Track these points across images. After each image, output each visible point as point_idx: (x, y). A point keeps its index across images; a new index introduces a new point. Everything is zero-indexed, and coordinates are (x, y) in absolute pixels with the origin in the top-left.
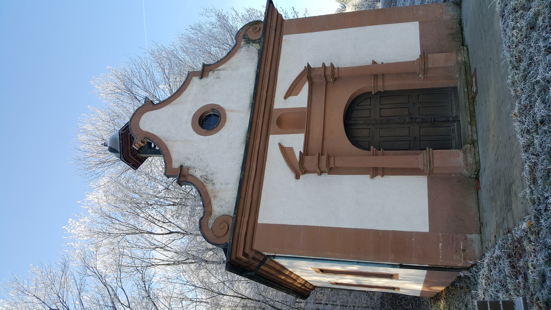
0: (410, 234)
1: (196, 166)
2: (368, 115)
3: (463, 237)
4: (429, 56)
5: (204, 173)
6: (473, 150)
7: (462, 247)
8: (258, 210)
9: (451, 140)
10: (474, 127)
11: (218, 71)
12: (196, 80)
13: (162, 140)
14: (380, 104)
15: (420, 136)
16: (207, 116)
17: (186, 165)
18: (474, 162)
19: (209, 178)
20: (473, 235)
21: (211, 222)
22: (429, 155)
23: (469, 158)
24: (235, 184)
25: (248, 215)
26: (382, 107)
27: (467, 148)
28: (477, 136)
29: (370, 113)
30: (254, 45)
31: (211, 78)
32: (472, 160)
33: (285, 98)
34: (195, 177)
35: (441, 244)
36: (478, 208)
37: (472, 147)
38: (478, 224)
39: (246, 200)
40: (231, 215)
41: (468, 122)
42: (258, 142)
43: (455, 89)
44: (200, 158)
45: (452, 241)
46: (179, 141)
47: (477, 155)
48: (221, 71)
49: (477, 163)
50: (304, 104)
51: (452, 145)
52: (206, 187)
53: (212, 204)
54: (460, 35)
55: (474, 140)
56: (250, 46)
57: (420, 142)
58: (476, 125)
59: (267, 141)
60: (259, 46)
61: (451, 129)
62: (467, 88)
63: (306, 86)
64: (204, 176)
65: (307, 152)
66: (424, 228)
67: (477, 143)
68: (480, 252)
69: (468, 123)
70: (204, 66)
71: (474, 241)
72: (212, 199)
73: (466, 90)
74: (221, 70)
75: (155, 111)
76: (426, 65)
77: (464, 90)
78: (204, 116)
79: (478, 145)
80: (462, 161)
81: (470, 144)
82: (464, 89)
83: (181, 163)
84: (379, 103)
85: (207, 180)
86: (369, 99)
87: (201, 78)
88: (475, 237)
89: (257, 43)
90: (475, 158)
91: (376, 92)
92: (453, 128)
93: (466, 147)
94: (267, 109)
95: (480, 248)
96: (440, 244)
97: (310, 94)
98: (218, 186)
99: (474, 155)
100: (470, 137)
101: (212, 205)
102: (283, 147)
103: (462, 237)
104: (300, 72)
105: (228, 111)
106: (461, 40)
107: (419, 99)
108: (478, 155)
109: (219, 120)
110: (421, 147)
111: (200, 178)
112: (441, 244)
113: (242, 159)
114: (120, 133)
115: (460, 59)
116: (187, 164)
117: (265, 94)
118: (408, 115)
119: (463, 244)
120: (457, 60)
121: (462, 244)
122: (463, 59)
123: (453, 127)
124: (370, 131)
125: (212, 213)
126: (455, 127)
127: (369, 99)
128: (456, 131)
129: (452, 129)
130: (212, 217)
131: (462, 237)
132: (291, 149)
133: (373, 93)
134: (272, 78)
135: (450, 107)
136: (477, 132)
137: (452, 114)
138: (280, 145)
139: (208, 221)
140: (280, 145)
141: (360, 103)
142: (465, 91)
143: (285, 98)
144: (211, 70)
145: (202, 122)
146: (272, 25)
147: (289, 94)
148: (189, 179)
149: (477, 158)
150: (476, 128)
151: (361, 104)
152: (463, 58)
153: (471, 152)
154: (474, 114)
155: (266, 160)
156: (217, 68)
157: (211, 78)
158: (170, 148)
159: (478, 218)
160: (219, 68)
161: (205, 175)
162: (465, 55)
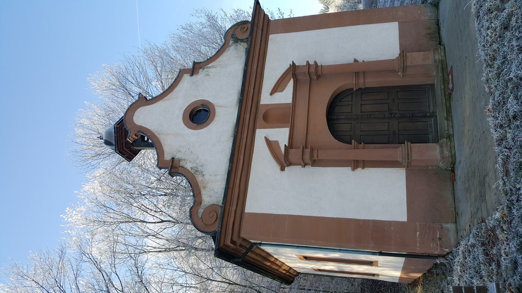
0: (389, 223)
1: (187, 158)
5: (195, 165)
6: (449, 143)
7: (438, 236)
8: (245, 200)
10: (450, 122)
11: (208, 69)
13: (155, 133)
14: (361, 100)
17: (177, 157)
18: (450, 155)
19: (199, 169)
20: (449, 224)
21: (201, 211)
22: (408, 148)
26: (363, 103)
27: (443, 142)
28: (453, 131)
30: (242, 44)
31: (201, 75)
35: (418, 233)
36: (453, 199)
38: (454, 214)
42: (245, 136)
43: (432, 86)
44: (190, 151)
48: (210, 69)
49: (453, 156)
50: (289, 100)
52: (196, 178)
53: (201, 194)
54: (438, 35)
56: (238, 44)
57: (399, 136)
61: (429, 123)
63: (291, 83)
67: (452, 137)
68: (455, 240)
70: (195, 63)
71: (449, 230)
72: (202, 190)
73: (442, 87)
74: (210, 68)
79: (454, 139)
81: (446, 139)
85: (197, 171)
86: (351, 96)
87: (192, 75)
88: (451, 226)
89: (245, 42)
93: (442, 142)
94: (254, 104)
95: (456, 237)
97: (295, 90)
98: (207, 177)
100: (446, 132)
101: (202, 195)
102: (269, 140)
103: (438, 226)
105: (217, 106)
110: (400, 141)
111: (190, 170)
112: (418, 233)
113: (231, 151)
115: (437, 57)
116: (178, 156)
117: (252, 90)
119: (439, 233)
121: (438, 233)
122: (440, 58)
124: (351, 125)
125: (202, 202)
127: (351, 96)
129: (429, 124)
131: (438, 226)
132: (277, 142)
133: (355, 90)
135: (427, 103)
136: (452, 127)
137: (430, 110)
138: (267, 139)
140: (267, 139)
141: (341, 100)
144: (201, 68)
148: (180, 170)
149: (453, 152)
154: (450, 110)
157: (201, 75)
161: (195, 167)
162: (442, 54)
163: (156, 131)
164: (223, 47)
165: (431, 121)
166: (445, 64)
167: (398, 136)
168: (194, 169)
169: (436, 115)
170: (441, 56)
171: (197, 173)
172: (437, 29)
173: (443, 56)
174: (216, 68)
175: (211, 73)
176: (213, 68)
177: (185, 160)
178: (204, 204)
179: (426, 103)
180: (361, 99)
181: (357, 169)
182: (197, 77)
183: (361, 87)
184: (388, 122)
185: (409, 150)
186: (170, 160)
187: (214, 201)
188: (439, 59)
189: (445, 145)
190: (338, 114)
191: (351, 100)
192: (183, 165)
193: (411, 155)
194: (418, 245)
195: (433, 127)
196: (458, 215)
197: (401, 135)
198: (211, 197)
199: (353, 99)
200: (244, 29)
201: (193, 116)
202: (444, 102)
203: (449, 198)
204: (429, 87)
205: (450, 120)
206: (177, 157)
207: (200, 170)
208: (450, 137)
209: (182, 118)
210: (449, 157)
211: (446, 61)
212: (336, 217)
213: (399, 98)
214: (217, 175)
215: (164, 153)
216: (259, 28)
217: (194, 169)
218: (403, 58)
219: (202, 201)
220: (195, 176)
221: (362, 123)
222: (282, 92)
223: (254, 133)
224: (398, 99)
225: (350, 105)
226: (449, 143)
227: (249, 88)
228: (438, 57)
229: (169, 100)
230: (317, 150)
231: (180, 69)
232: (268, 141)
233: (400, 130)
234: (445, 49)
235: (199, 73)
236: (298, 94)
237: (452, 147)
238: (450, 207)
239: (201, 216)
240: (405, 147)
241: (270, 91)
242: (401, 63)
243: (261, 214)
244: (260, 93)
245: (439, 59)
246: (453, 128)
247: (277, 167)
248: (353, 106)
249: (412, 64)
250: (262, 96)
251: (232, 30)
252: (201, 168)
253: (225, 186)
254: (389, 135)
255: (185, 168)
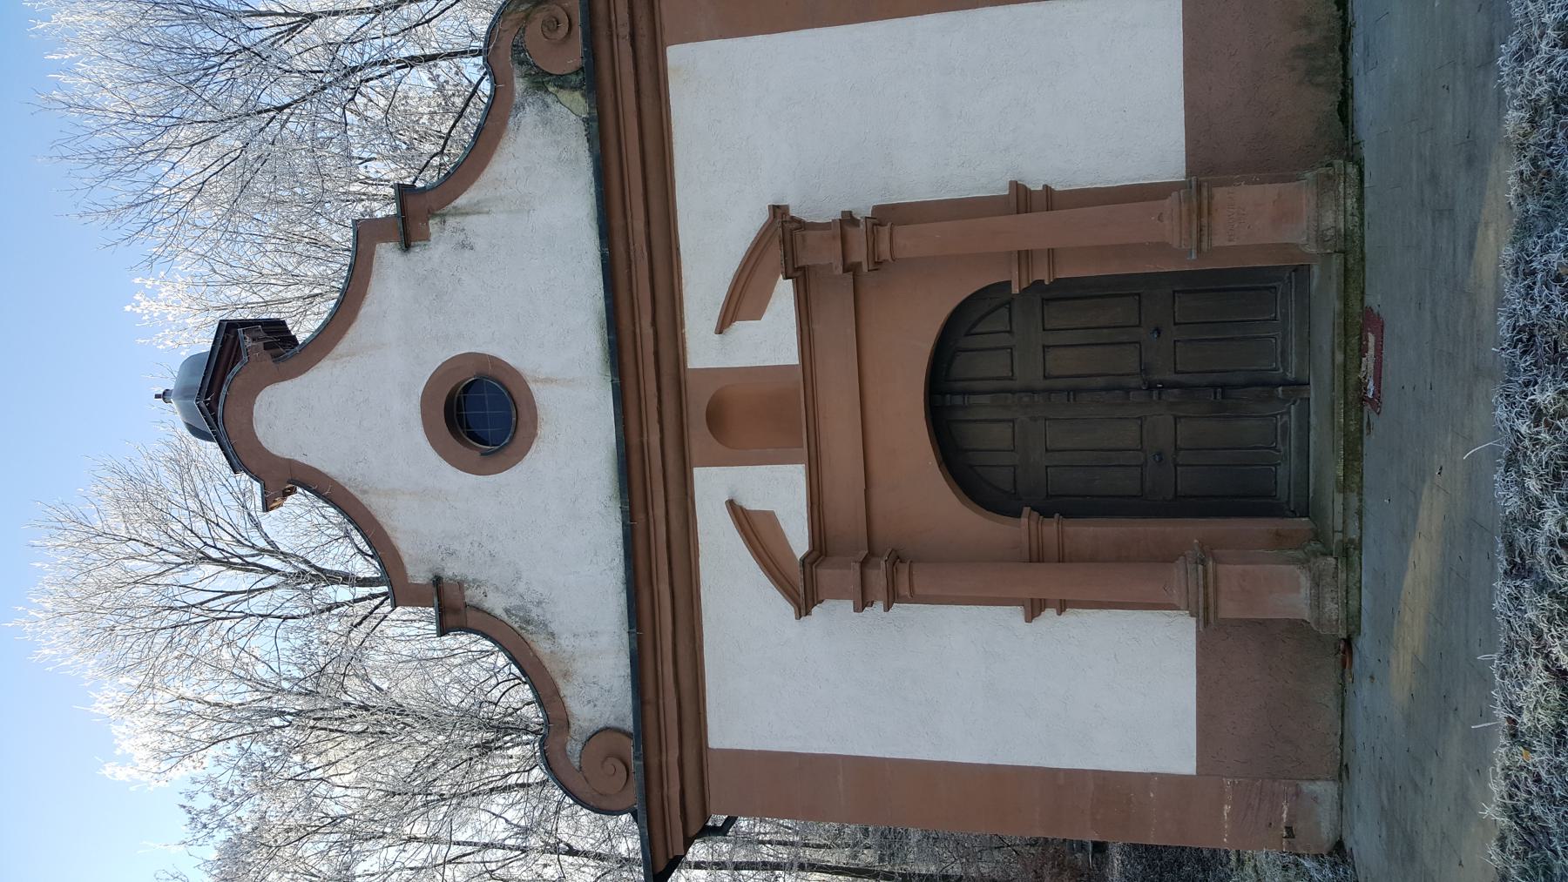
0: (1145, 780)
1: (482, 578)
2: (1006, 372)
3: (1290, 789)
4: (1220, 194)
5: (514, 602)
6: (1342, 576)
7: (1284, 816)
8: (702, 712)
9: (1275, 465)
10: (1355, 494)
11: (458, 219)
12: (387, 254)
13: (347, 487)
14: (1044, 330)
15: (1177, 449)
16: (466, 385)
17: (450, 574)
18: (1342, 616)
19: (533, 615)
20: (1319, 783)
21: (574, 747)
22: (1206, 587)
23: (1327, 603)
24: (619, 636)
25: (666, 567)
26: (1051, 339)
27: (1324, 570)
28: (1361, 528)
29: (1009, 362)
30: (565, 95)
31: (438, 249)
32: (1338, 609)
33: (720, 329)
34: (489, 614)
35: (1227, 808)
36: (1340, 709)
37: (1339, 566)
38: (1337, 754)
39: (661, 702)
40: (626, 727)
41: (1337, 482)
42: (659, 512)
43: (1301, 272)
44: (487, 553)
45: (1260, 799)
46: (403, 493)
47: (1354, 591)
48: (469, 218)
49: (1352, 618)
50: (787, 353)
51: (1276, 483)
52: (532, 645)
53: (562, 695)
54: (1337, 56)
55: (1349, 540)
56: (549, 100)
58: (1361, 488)
59: (689, 493)
60: (582, 101)
61: (1279, 424)
62: (1345, 353)
63: (784, 291)
64: (514, 609)
65: (819, 517)
66: (1184, 762)
67: (1357, 552)
68: (1332, 827)
69: (1337, 486)
70: (404, 193)
71: (1319, 801)
72: (560, 683)
73: (1339, 358)
74: (467, 214)
75: (289, 381)
76: (1205, 238)
77: (1333, 360)
78: (460, 389)
79: (1361, 559)
80: (1306, 604)
81: (1336, 559)
82: (1333, 353)
83: (431, 566)
84: (1040, 324)
85: (528, 622)
86: (1004, 311)
87: (406, 246)
88: (1324, 789)
89: (574, 88)
90: (1347, 603)
91: (1025, 285)
92: (1286, 422)
93: (1321, 567)
94: (667, 381)
95: (1336, 818)
96: (1226, 807)
97: (804, 313)
98: (565, 641)
99: (1344, 593)
100: (1339, 536)
101: (564, 699)
102: (741, 508)
103: (1288, 788)
104: (752, 236)
105: (536, 381)
106: (1339, 80)
107: (1176, 310)
108: (1357, 591)
109: (514, 419)
110: (1179, 488)
111: (505, 617)
112: (1227, 808)
113: (622, 553)
114: (203, 405)
115: (1329, 219)
116: (452, 570)
117: (648, 331)
118: (1139, 371)
119: (1289, 809)
120: (1318, 226)
121: (1285, 807)
122: (1342, 225)
123: (1286, 418)
125: (571, 720)
126: (1290, 416)
128: (1292, 432)
129: (1282, 425)
130: (572, 733)
131: (1288, 788)
132: (770, 516)
133: (1015, 290)
134: (652, 159)
135: (1279, 341)
136: (1360, 513)
137: (1285, 370)
138: (732, 505)
139: (565, 745)
140: (732, 505)
141: (974, 325)
142: (1337, 362)
143: (720, 329)
144: (431, 214)
145: (457, 410)
146: (613, 18)
147: (730, 315)
148: (472, 619)
149: (1353, 603)
150: (1361, 500)
151: (979, 329)
152: (1341, 217)
153: (1337, 581)
154: (1359, 448)
155: (697, 556)
156: (450, 206)
157: (441, 248)
158: (381, 519)
159: (1339, 737)
160: (462, 201)
161: (520, 608)
162: (1349, 202)
163: (349, 480)
164: (492, 112)
165: (1289, 413)
166: (1358, 250)
167: (1173, 469)
168: (516, 616)
169: (1306, 396)
170: (1345, 211)
171: (529, 628)
172: (1337, 24)
173: (1352, 215)
174: (488, 213)
175: (478, 235)
176: (479, 213)
177: (477, 583)
178: (577, 727)
179: (1274, 341)
180: (1043, 326)
181: (1039, 615)
182: (427, 254)
183: (1038, 277)
184: (1139, 418)
185: (1211, 590)
186: (428, 584)
187: (607, 716)
188: (1337, 231)
189: (1328, 580)
190: (966, 384)
191: (1008, 329)
192: (475, 601)
193: (1216, 607)
194: (1225, 840)
195: (1292, 438)
196: (1348, 777)
197: (1182, 465)
198: (595, 706)
199: (1014, 325)
200: (559, 31)
201: (459, 408)
202: (1339, 422)
203: (1327, 707)
204: (1287, 275)
205: (1352, 485)
206: (450, 573)
207: (536, 618)
208: (1349, 552)
209: (421, 428)
210: (1337, 623)
211: (1362, 237)
212: (984, 761)
213: (1177, 321)
214: (596, 632)
215: (399, 558)
216: (617, 36)
217: (516, 616)
218: (1200, 216)
219: (569, 718)
220: (526, 639)
221: (1051, 419)
222: (759, 318)
223: (689, 482)
224: (1175, 324)
225: (1003, 348)
226: (1344, 576)
227: (637, 325)
228: (1332, 220)
229: (354, 354)
230: (911, 562)
231: (355, 222)
232: (741, 516)
233: (1181, 449)
234: (1362, 181)
235: (432, 238)
236: (816, 327)
237: (1350, 584)
238: (1328, 734)
239: (578, 764)
240: (1198, 576)
241: (714, 324)
242: (1191, 236)
243: (760, 752)
244: (679, 322)
245: (1337, 231)
246: (1360, 519)
247: (790, 610)
248: (1016, 354)
249: (1230, 241)
250: (687, 336)
251: (508, 25)
252: (540, 611)
253: (629, 670)
254: (1141, 466)
255: (485, 612)
